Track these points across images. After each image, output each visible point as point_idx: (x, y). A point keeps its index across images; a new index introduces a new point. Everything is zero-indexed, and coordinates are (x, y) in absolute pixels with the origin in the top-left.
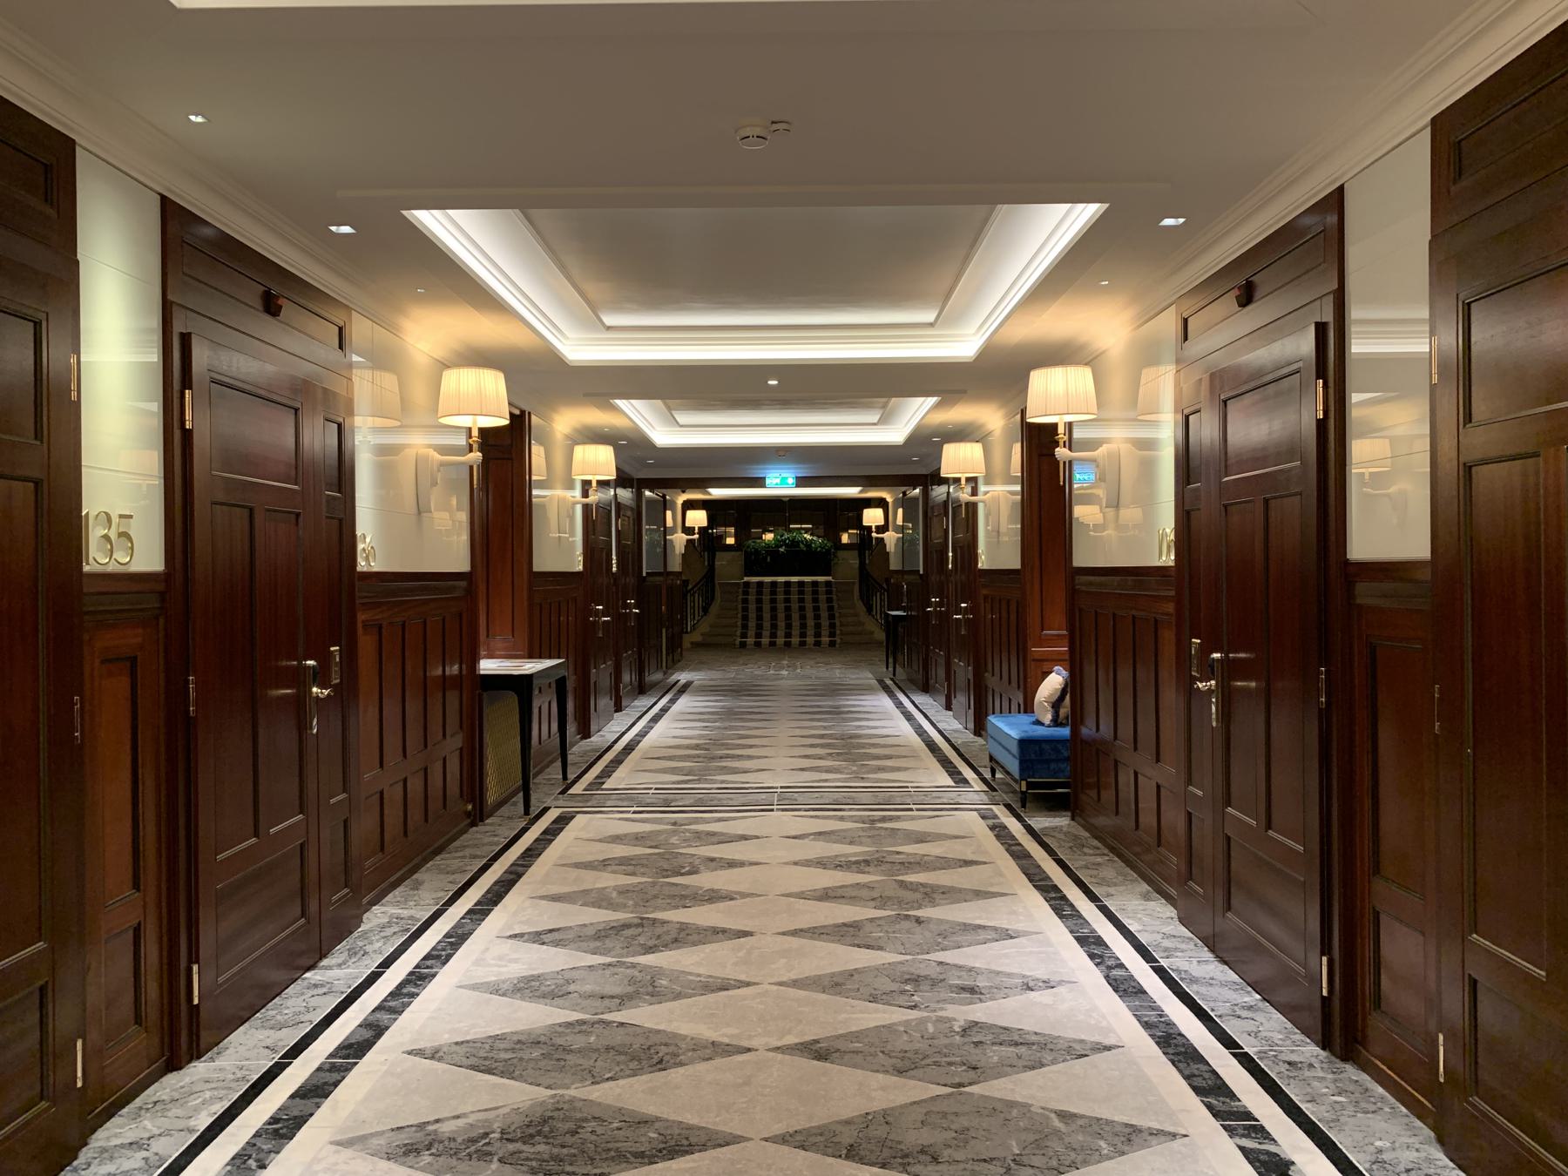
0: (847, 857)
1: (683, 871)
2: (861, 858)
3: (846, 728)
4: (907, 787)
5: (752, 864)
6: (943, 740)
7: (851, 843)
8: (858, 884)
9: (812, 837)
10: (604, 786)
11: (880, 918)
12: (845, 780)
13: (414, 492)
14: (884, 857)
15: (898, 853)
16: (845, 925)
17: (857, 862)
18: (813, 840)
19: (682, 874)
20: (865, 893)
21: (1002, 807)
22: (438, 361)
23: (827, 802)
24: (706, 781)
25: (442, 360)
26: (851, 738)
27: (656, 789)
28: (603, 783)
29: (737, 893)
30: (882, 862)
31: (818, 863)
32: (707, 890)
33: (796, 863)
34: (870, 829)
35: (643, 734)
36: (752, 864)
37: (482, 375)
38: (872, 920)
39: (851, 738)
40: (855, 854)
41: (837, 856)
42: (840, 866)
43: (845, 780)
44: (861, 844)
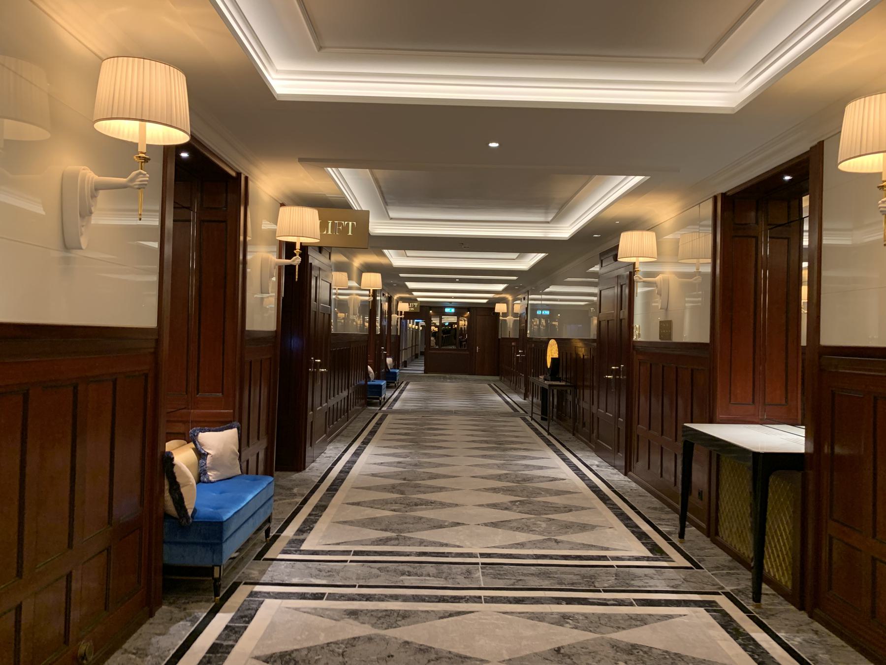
0: (426, 508)
1: (519, 503)
2: (419, 507)
3: (516, 468)
4: (604, 558)
5: (482, 505)
6: (600, 481)
7: (421, 518)
8: (425, 493)
9: (446, 524)
10: (304, 547)
11: (420, 480)
12: (534, 544)
13: (260, 283)
14: (405, 507)
15: (394, 510)
16: (435, 479)
17: (421, 505)
18: (445, 521)
19: (518, 501)
20: (422, 489)
21: (723, 596)
22: (275, 200)
23: (310, 564)
24: (407, 541)
25: (276, 198)
26: (524, 480)
27: (356, 553)
28: (303, 541)
29: (483, 491)
30: (407, 505)
31: (444, 505)
32: (499, 493)
33: (457, 505)
34: (401, 531)
35: (351, 463)
36: (482, 505)
37: (292, 210)
38: (424, 480)
39: (524, 480)
40: (422, 510)
41: (432, 509)
42: (432, 503)
43: (534, 544)
44: (414, 518)
